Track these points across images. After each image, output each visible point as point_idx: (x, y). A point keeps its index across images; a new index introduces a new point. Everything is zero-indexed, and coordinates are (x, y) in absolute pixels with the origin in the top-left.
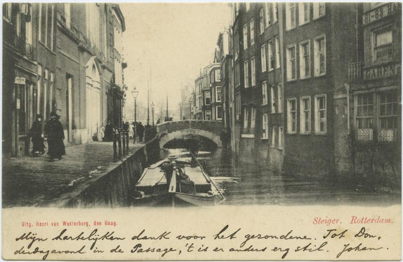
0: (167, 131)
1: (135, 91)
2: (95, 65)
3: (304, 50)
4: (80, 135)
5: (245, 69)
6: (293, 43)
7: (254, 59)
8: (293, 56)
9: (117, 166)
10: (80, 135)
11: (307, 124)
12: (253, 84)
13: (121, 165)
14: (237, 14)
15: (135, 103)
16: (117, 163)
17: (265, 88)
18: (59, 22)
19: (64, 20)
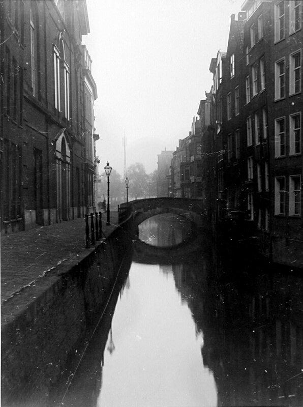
0: (142, 209)
1: (108, 167)
2: (65, 139)
3: (279, 126)
4: (197, 339)
5: (248, 139)
6: (299, 111)
7: (231, 136)
8: (282, 130)
9: (89, 253)
10: (197, 339)
11: (281, 205)
12: (292, 152)
13: (93, 252)
14: (221, 82)
15: (108, 181)
16: (89, 249)
17: (250, 164)
18: (27, 93)
19: (31, 89)
